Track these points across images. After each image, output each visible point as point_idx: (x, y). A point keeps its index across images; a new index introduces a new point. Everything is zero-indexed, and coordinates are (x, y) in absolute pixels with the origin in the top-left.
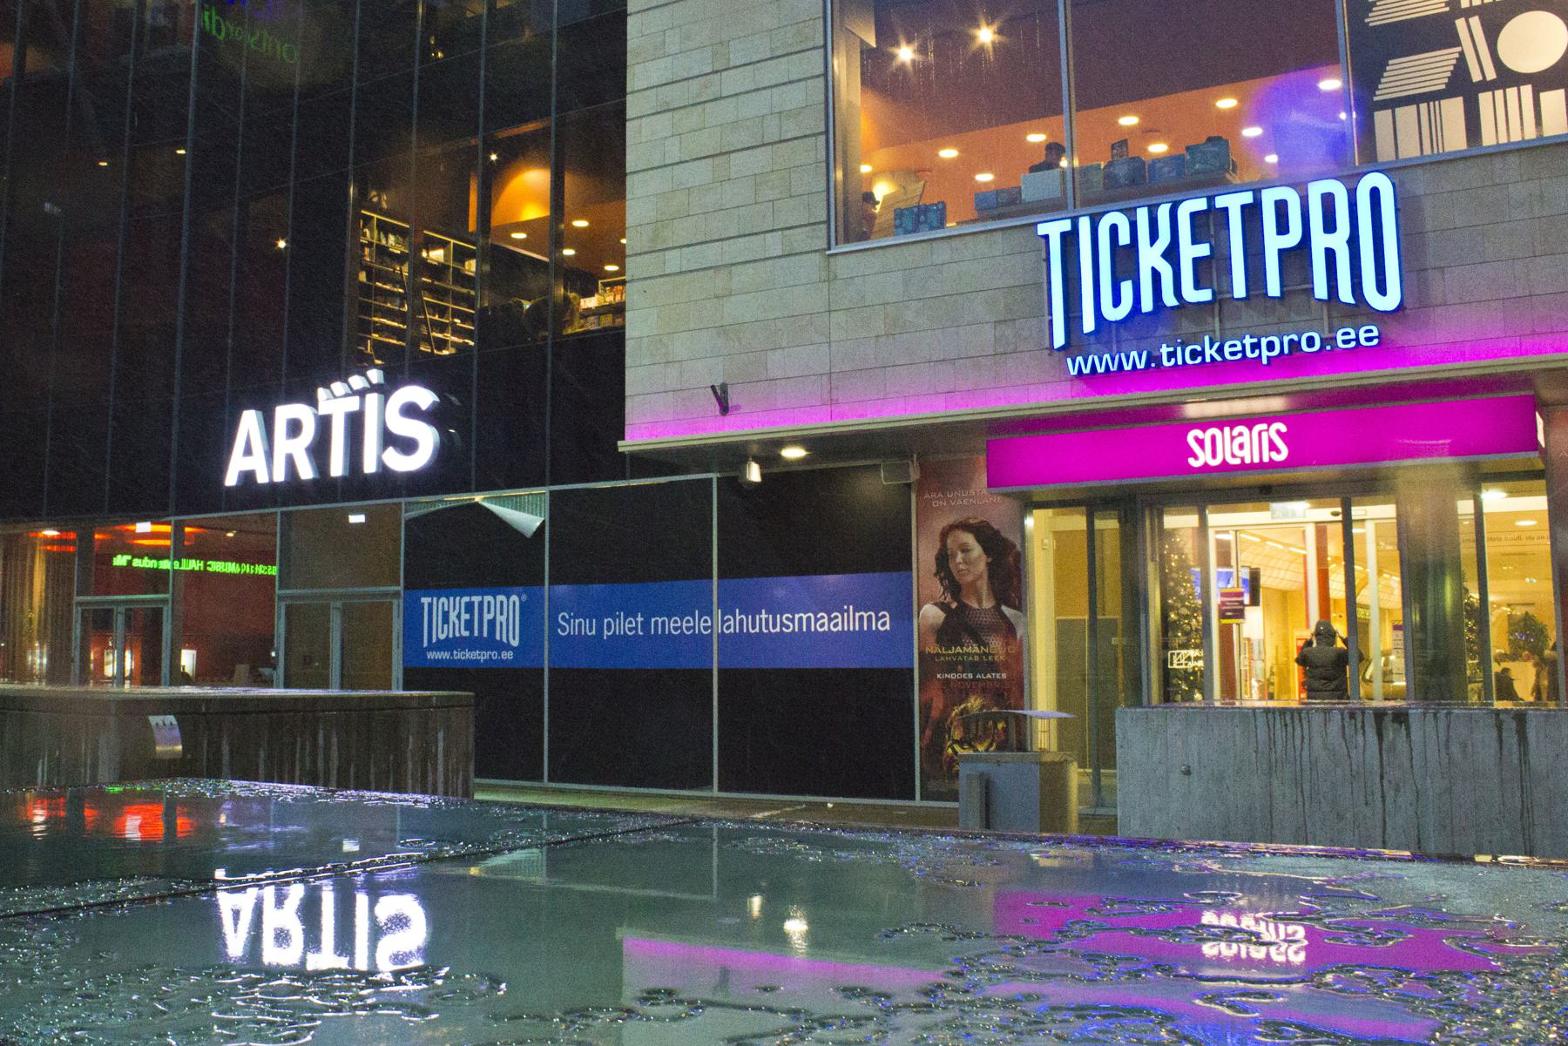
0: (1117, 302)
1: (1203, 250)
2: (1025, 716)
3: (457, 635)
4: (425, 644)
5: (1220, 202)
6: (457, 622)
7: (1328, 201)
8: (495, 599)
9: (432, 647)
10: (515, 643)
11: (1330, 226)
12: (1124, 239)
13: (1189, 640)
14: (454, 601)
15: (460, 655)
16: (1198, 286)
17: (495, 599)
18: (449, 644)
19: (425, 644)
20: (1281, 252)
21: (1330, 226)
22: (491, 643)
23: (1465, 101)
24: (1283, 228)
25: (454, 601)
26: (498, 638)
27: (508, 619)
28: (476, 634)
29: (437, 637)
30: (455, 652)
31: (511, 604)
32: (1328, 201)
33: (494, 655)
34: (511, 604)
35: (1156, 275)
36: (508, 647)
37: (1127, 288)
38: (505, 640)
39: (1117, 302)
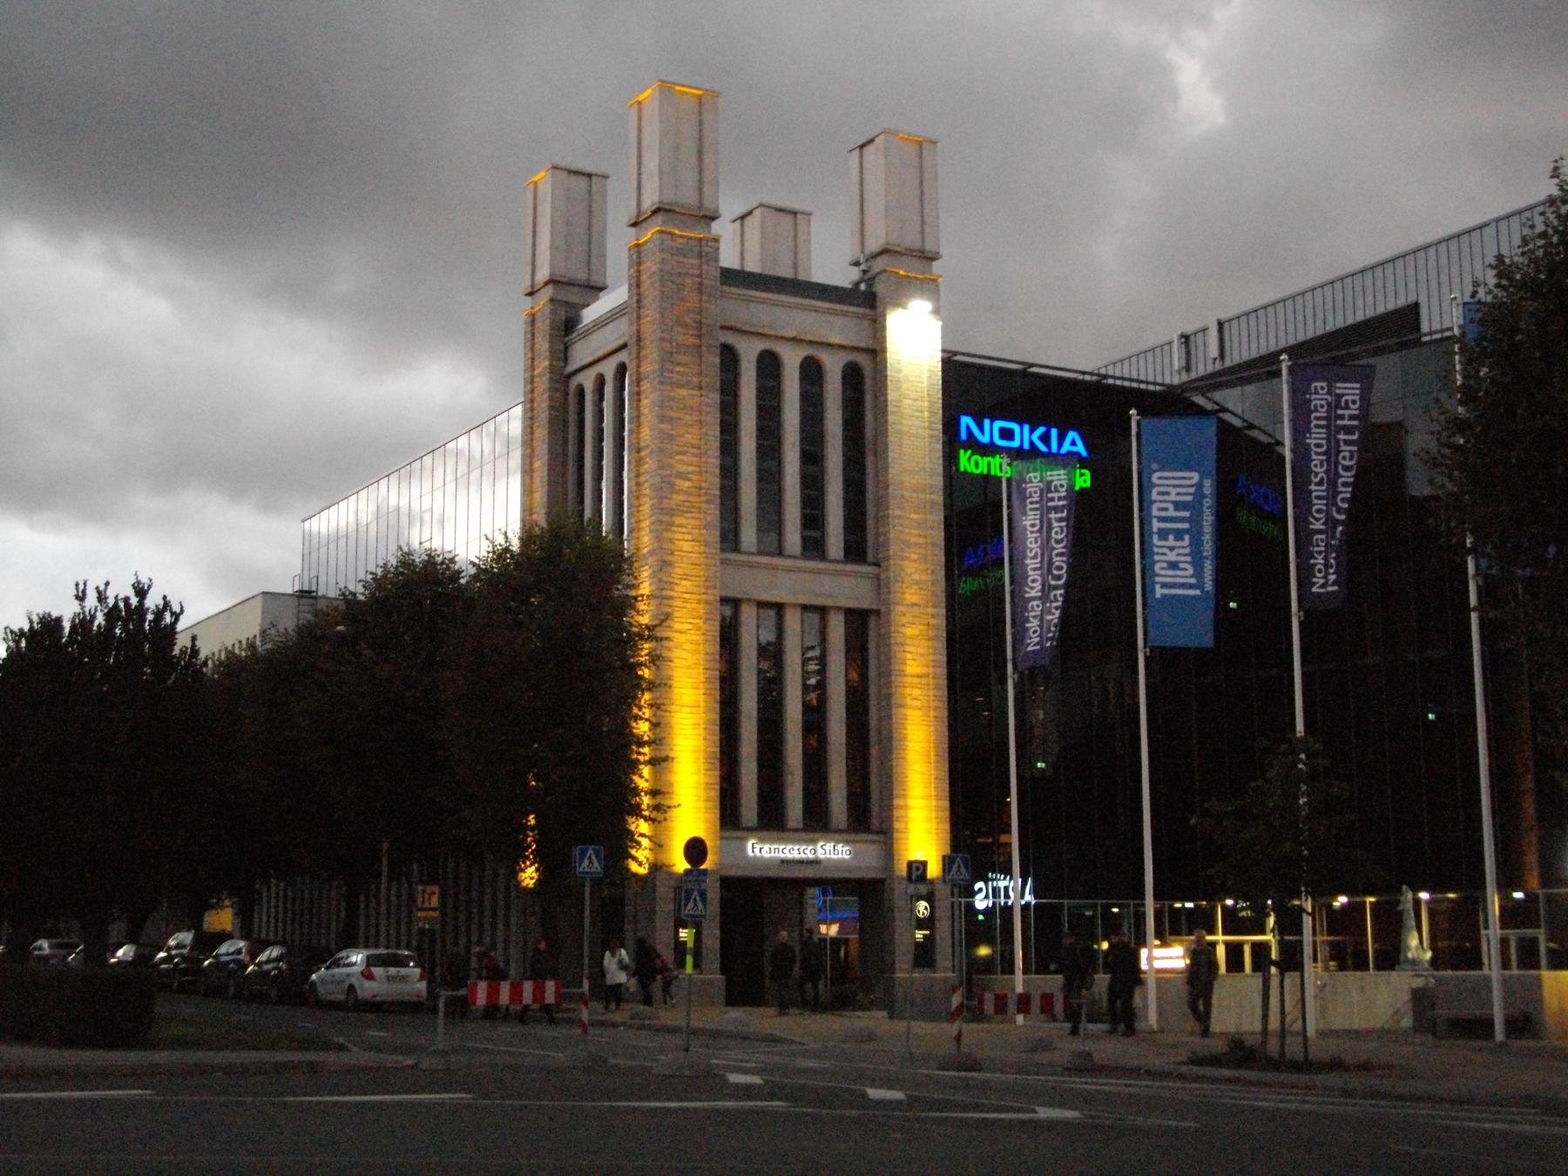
0: (1185, 569)
1: (1171, 537)
2: (1328, 935)
3: (1187, 551)
4: (1198, 592)
5: (1155, 530)
6: (1176, 551)
7: (1160, 493)
8: (1155, 501)
9: (1200, 586)
10: (1196, 476)
11: (1168, 494)
12: (1165, 565)
13: (1327, 580)
14: (1158, 554)
15: (1208, 548)
16: (1183, 540)
17: (1155, 501)
18: (1197, 563)
19: (1198, 592)
20: (1175, 510)
21: (1168, 494)
22: (1194, 506)
23: (1200, 652)
24: (1166, 509)
25: (1158, 554)
26: (1190, 498)
27: (1174, 486)
28: (1186, 526)
29: (1192, 576)
30: (1205, 554)
31: (1161, 482)
32: (1160, 493)
33: (1208, 502)
34: (1161, 482)
35: (1179, 555)
36: (1199, 486)
37: (1182, 566)
38: (1192, 490)
39: (1185, 569)
